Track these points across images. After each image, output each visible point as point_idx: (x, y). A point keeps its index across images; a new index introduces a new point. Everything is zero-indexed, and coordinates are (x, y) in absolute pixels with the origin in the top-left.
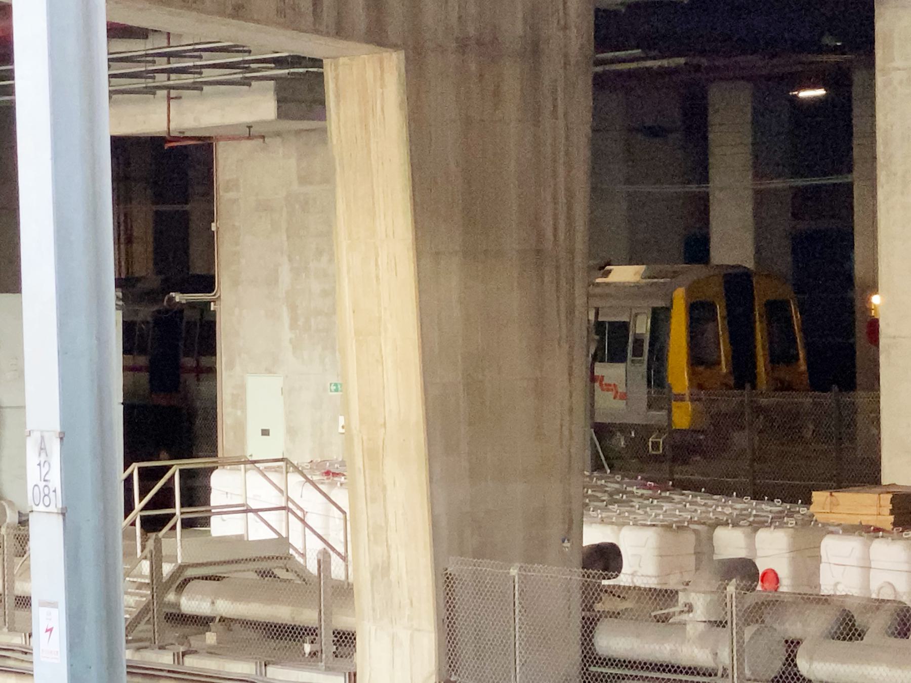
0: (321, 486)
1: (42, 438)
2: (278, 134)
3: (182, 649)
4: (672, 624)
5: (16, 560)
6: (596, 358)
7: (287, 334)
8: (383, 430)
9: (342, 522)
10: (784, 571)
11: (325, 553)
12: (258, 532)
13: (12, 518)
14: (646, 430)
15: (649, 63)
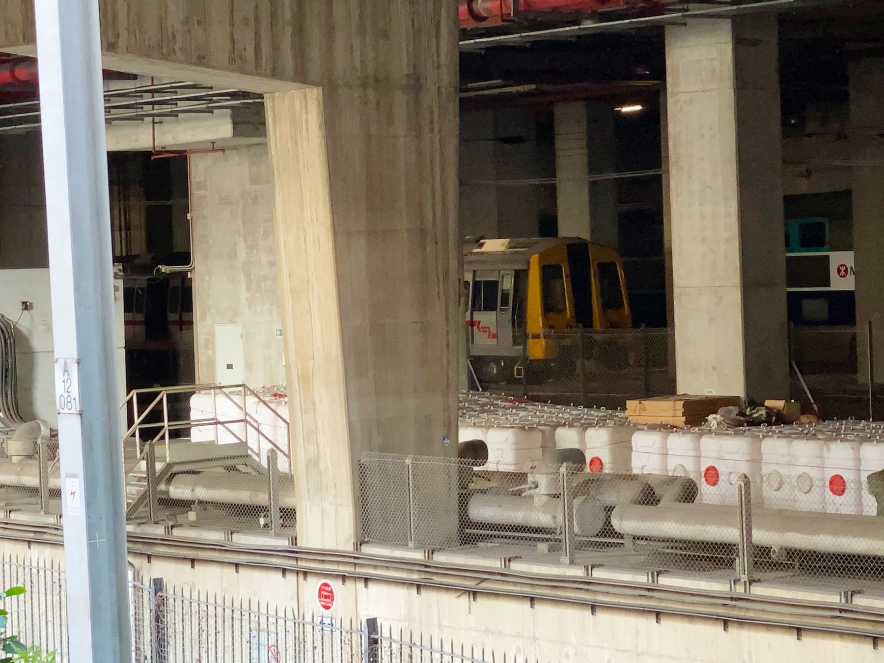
1: (65, 363)
2: (234, 148)
3: (171, 523)
4: (525, 497)
5: (49, 463)
7: (244, 294)
8: (312, 362)
10: (606, 459)
11: (272, 451)
12: (225, 438)
13: (45, 431)
14: (511, 361)
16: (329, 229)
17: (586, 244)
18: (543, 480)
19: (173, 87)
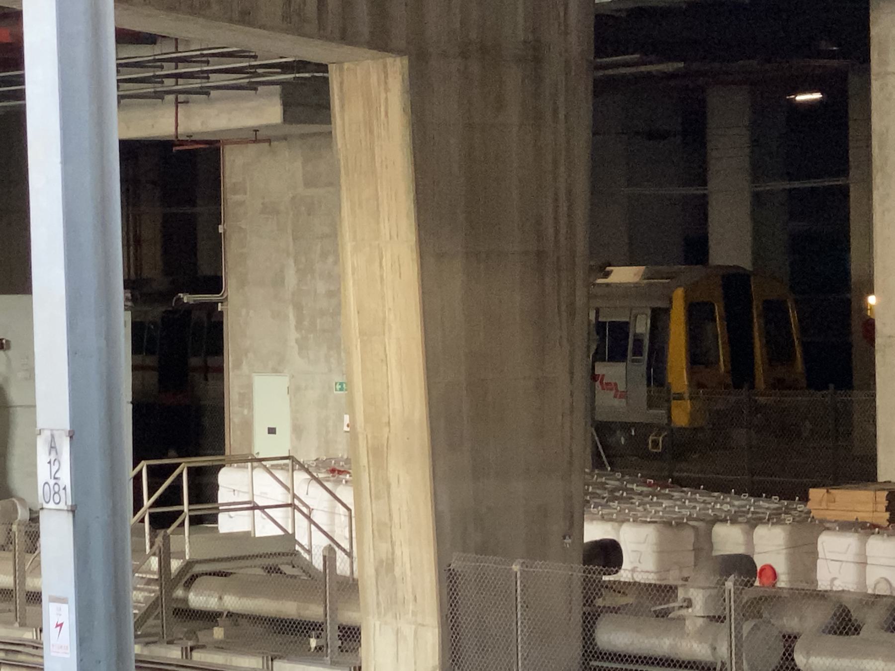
0: (326, 484)
1: (53, 436)
3: (190, 643)
5: (28, 556)
6: (599, 356)
7: (293, 335)
9: (347, 519)
10: (781, 566)
12: (265, 529)
13: (22, 514)
14: (645, 428)
15: (643, 69)
16: (414, 247)
17: (749, 276)
18: (698, 597)
19: (203, 55)
